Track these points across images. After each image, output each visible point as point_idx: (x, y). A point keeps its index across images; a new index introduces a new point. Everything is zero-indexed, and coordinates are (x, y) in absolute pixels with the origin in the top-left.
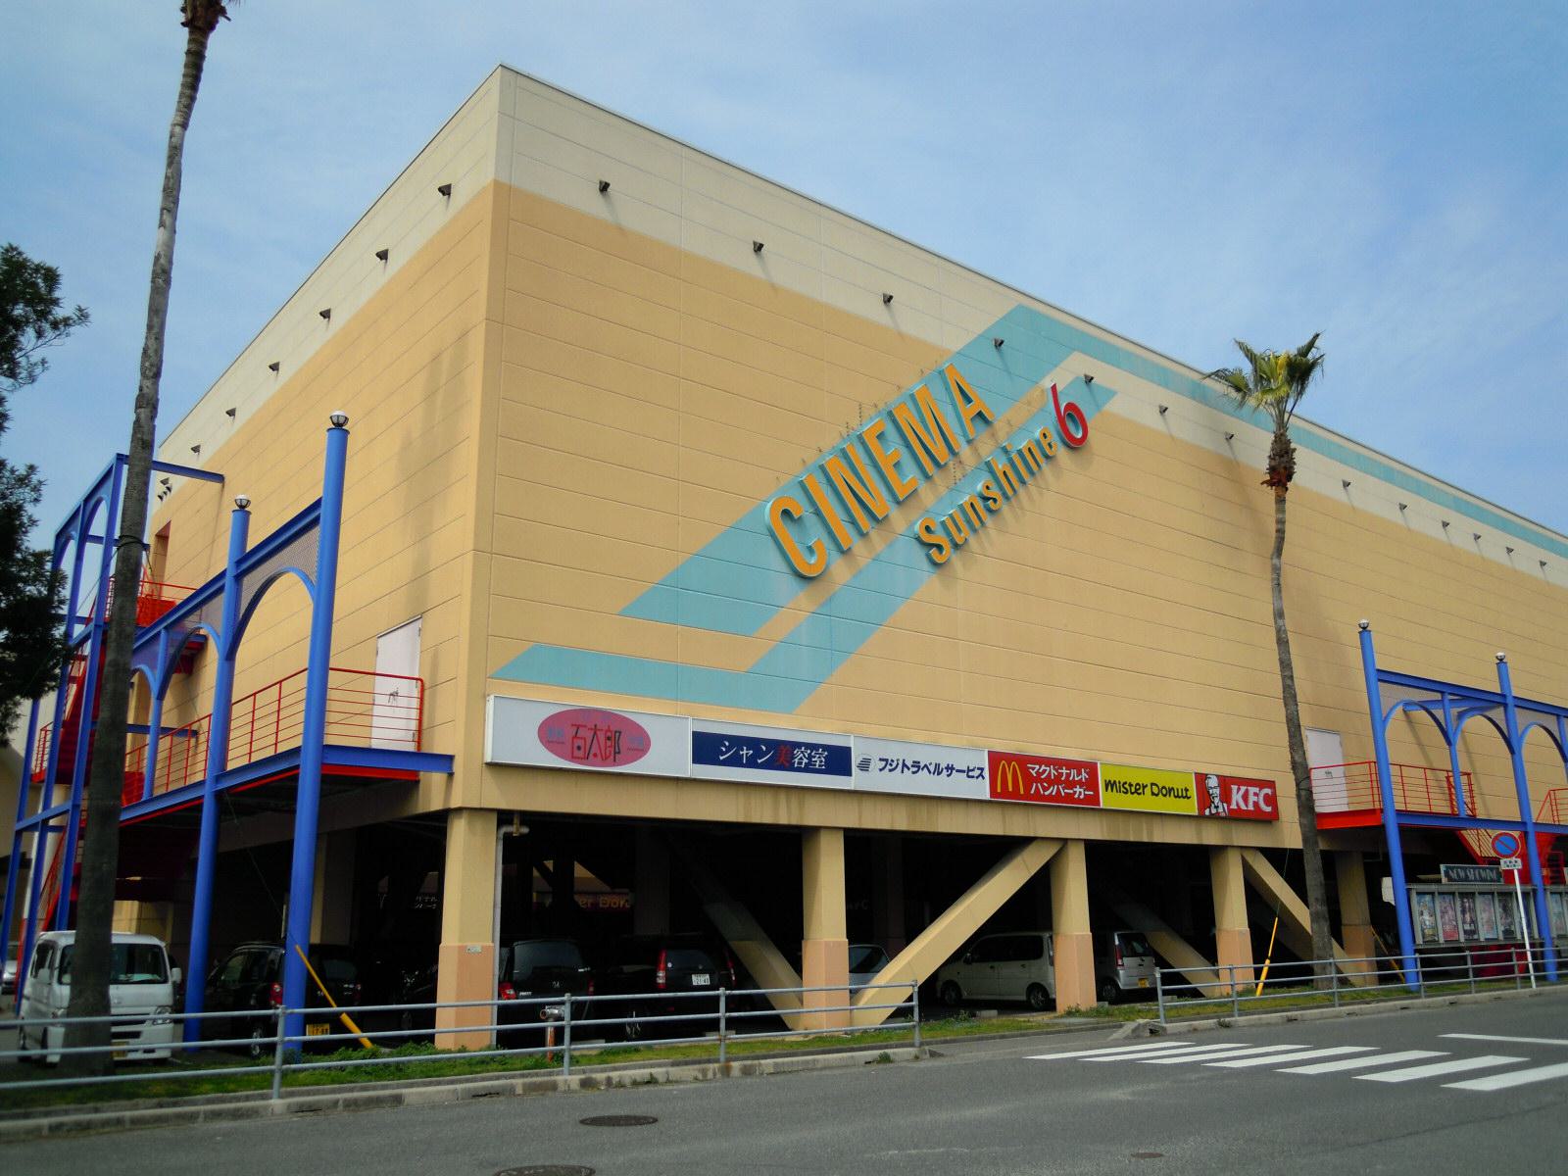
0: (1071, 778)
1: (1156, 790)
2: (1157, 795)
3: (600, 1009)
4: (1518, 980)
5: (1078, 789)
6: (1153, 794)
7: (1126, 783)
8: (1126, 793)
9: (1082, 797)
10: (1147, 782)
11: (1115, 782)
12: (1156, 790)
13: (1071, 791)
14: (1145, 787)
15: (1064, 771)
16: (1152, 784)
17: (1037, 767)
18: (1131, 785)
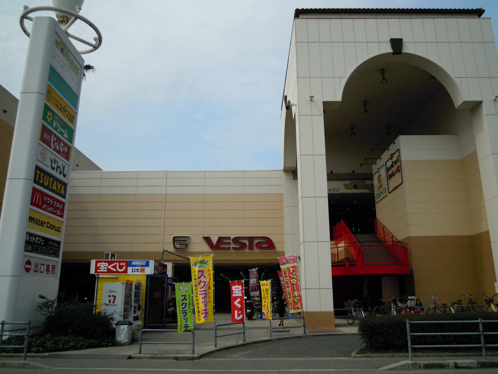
0: (57, 206)
1: (48, 226)
2: (49, 228)
3: (137, 295)
4: (484, 349)
5: (58, 211)
6: (47, 227)
7: (37, 219)
8: (37, 224)
9: (59, 214)
10: (46, 221)
11: (33, 218)
12: (48, 226)
13: (56, 211)
14: (45, 223)
15: (55, 202)
16: (48, 223)
17: (47, 198)
18: (39, 221)
